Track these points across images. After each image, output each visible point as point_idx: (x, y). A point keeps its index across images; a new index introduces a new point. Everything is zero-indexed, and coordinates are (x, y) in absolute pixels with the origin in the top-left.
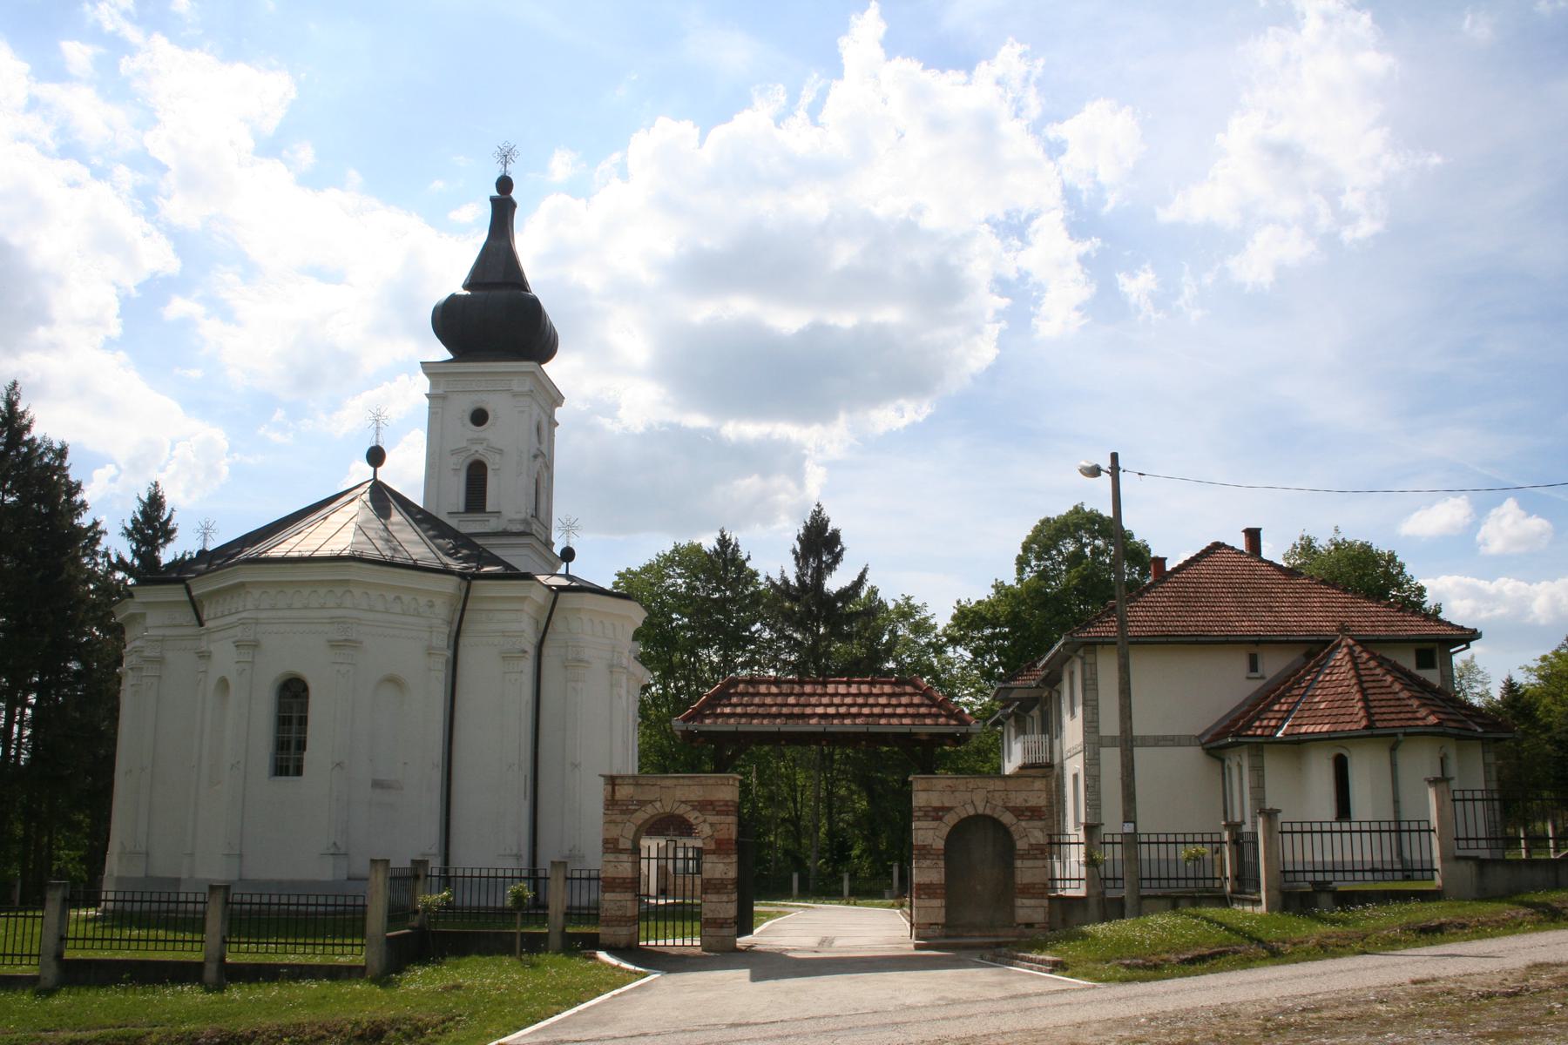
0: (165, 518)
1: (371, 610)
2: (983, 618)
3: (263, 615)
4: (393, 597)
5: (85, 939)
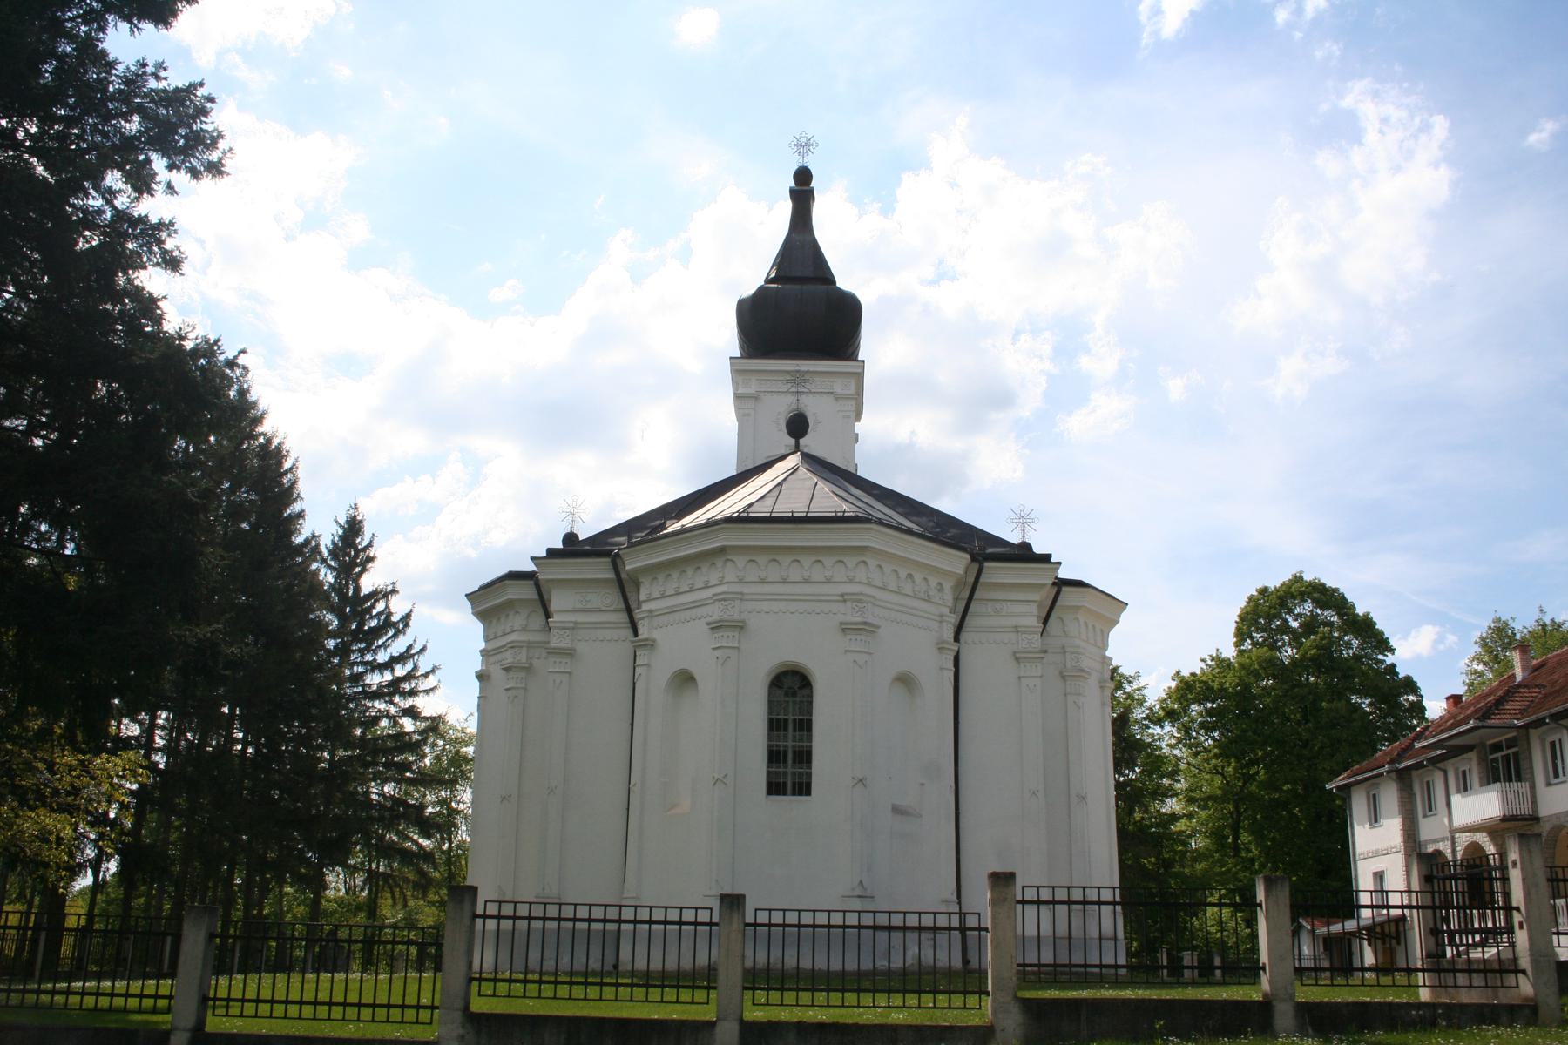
0: (364, 544)
1: (884, 589)
2: (1211, 689)
3: (746, 589)
4: (906, 574)
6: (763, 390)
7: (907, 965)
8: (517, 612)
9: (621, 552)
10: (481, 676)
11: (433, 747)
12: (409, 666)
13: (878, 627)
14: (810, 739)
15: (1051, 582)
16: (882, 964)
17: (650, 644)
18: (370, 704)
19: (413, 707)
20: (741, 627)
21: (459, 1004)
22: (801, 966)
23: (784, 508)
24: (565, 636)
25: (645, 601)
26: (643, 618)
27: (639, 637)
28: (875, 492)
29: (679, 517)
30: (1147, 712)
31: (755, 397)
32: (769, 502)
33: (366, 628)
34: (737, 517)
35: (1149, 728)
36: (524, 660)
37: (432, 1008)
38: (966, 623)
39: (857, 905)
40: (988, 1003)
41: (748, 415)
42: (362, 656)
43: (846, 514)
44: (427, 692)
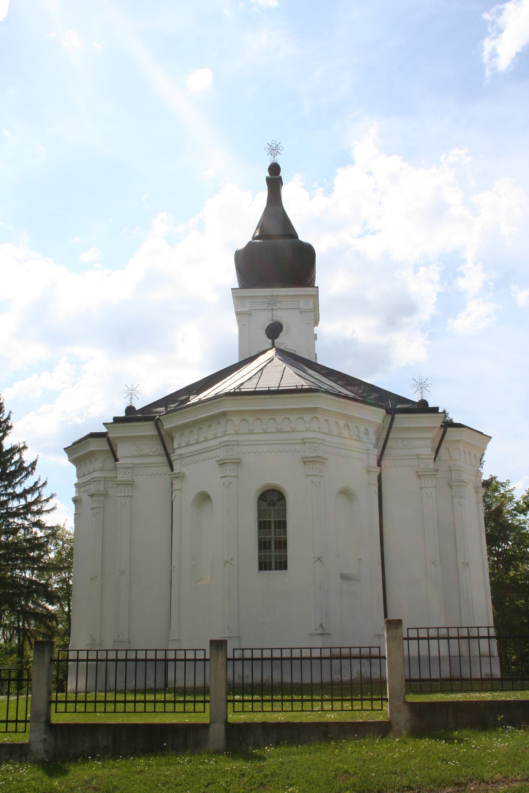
1: (330, 434)
3: (240, 438)
5: (17, 721)
6: (253, 308)
7: (353, 678)
8: (97, 459)
9: (160, 418)
10: (75, 501)
11: (56, 546)
12: (36, 495)
13: (327, 459)
14: (285, 533)
15: (439, 425)
16: (336, 677)
17: (181, 476)
18: (11, 520)
19: (39, 521)
20: (238, 463)
21: (43, 719)
22: (283, 681)
23: (263, 386)
24: (127, 473)
25: (177, 449)
26: (176, 460)
27: (174, 472)
28: (324, 372)
29: (198, 393)
30: (515, 505)
31: (249, 314)
32: (254, 381)
33: (8, 471)
34: (234, 392)
35: (517, 516)
36: (102, 489)
37: (26, 721)
38: (385, 453)
39: (319, 642)
40: (387, 707)
41: (245, 325)
42: (6, 489)
43: (304, 387)
44: (48, 511)
